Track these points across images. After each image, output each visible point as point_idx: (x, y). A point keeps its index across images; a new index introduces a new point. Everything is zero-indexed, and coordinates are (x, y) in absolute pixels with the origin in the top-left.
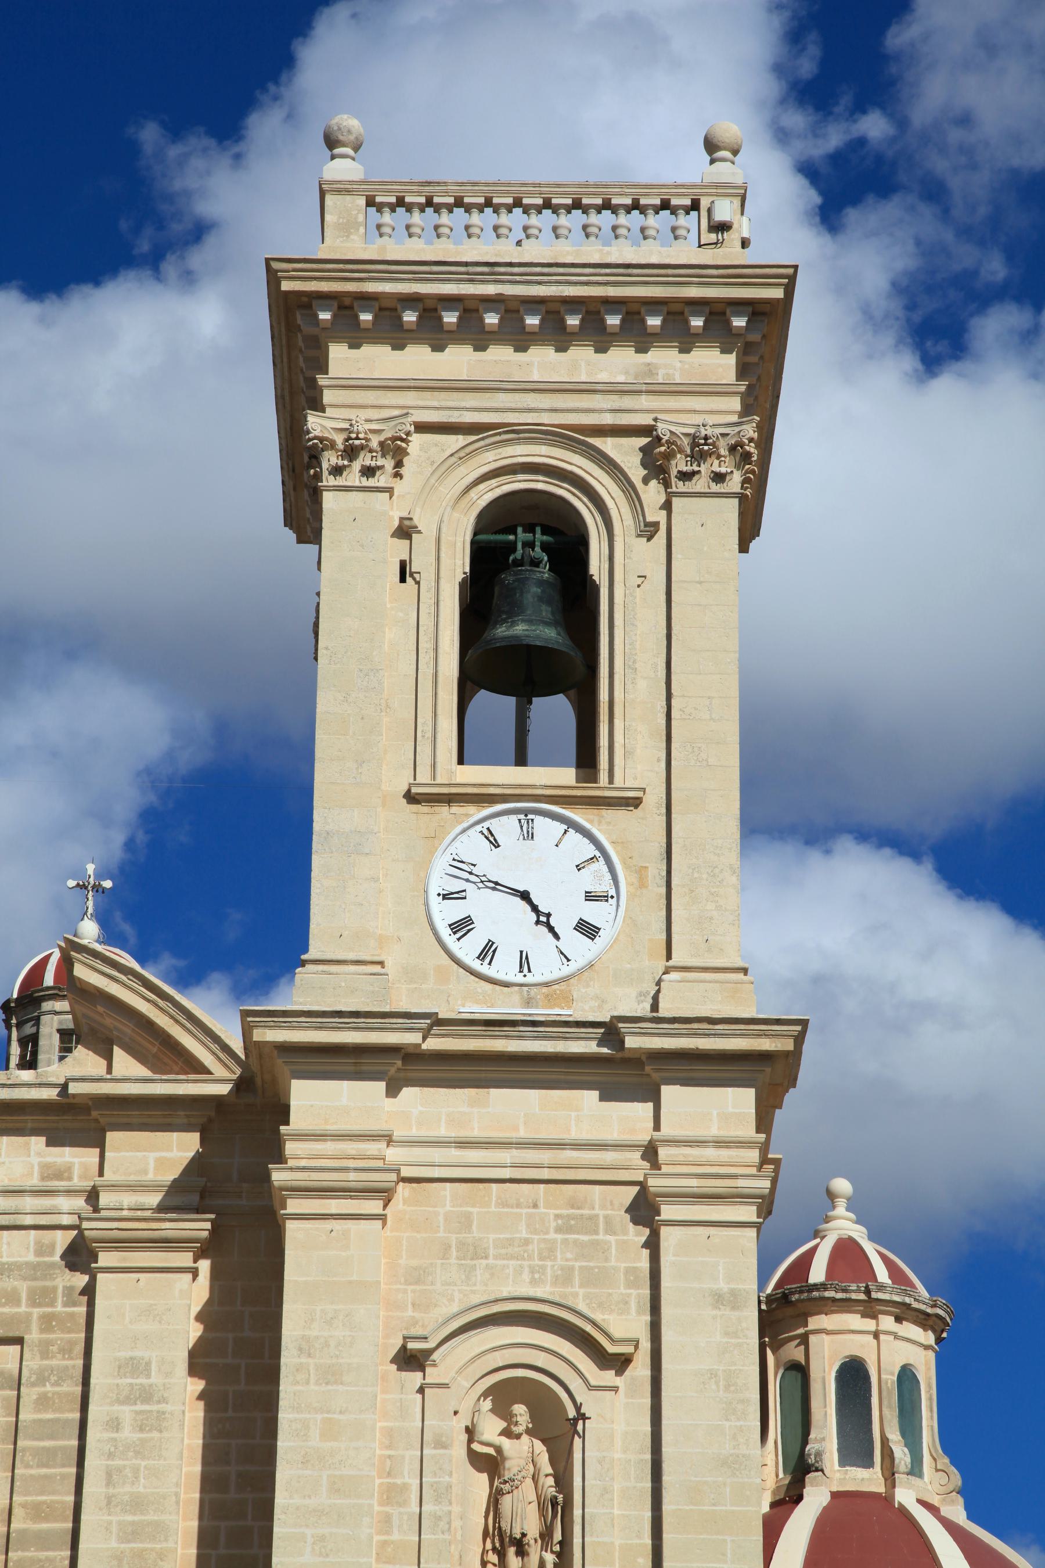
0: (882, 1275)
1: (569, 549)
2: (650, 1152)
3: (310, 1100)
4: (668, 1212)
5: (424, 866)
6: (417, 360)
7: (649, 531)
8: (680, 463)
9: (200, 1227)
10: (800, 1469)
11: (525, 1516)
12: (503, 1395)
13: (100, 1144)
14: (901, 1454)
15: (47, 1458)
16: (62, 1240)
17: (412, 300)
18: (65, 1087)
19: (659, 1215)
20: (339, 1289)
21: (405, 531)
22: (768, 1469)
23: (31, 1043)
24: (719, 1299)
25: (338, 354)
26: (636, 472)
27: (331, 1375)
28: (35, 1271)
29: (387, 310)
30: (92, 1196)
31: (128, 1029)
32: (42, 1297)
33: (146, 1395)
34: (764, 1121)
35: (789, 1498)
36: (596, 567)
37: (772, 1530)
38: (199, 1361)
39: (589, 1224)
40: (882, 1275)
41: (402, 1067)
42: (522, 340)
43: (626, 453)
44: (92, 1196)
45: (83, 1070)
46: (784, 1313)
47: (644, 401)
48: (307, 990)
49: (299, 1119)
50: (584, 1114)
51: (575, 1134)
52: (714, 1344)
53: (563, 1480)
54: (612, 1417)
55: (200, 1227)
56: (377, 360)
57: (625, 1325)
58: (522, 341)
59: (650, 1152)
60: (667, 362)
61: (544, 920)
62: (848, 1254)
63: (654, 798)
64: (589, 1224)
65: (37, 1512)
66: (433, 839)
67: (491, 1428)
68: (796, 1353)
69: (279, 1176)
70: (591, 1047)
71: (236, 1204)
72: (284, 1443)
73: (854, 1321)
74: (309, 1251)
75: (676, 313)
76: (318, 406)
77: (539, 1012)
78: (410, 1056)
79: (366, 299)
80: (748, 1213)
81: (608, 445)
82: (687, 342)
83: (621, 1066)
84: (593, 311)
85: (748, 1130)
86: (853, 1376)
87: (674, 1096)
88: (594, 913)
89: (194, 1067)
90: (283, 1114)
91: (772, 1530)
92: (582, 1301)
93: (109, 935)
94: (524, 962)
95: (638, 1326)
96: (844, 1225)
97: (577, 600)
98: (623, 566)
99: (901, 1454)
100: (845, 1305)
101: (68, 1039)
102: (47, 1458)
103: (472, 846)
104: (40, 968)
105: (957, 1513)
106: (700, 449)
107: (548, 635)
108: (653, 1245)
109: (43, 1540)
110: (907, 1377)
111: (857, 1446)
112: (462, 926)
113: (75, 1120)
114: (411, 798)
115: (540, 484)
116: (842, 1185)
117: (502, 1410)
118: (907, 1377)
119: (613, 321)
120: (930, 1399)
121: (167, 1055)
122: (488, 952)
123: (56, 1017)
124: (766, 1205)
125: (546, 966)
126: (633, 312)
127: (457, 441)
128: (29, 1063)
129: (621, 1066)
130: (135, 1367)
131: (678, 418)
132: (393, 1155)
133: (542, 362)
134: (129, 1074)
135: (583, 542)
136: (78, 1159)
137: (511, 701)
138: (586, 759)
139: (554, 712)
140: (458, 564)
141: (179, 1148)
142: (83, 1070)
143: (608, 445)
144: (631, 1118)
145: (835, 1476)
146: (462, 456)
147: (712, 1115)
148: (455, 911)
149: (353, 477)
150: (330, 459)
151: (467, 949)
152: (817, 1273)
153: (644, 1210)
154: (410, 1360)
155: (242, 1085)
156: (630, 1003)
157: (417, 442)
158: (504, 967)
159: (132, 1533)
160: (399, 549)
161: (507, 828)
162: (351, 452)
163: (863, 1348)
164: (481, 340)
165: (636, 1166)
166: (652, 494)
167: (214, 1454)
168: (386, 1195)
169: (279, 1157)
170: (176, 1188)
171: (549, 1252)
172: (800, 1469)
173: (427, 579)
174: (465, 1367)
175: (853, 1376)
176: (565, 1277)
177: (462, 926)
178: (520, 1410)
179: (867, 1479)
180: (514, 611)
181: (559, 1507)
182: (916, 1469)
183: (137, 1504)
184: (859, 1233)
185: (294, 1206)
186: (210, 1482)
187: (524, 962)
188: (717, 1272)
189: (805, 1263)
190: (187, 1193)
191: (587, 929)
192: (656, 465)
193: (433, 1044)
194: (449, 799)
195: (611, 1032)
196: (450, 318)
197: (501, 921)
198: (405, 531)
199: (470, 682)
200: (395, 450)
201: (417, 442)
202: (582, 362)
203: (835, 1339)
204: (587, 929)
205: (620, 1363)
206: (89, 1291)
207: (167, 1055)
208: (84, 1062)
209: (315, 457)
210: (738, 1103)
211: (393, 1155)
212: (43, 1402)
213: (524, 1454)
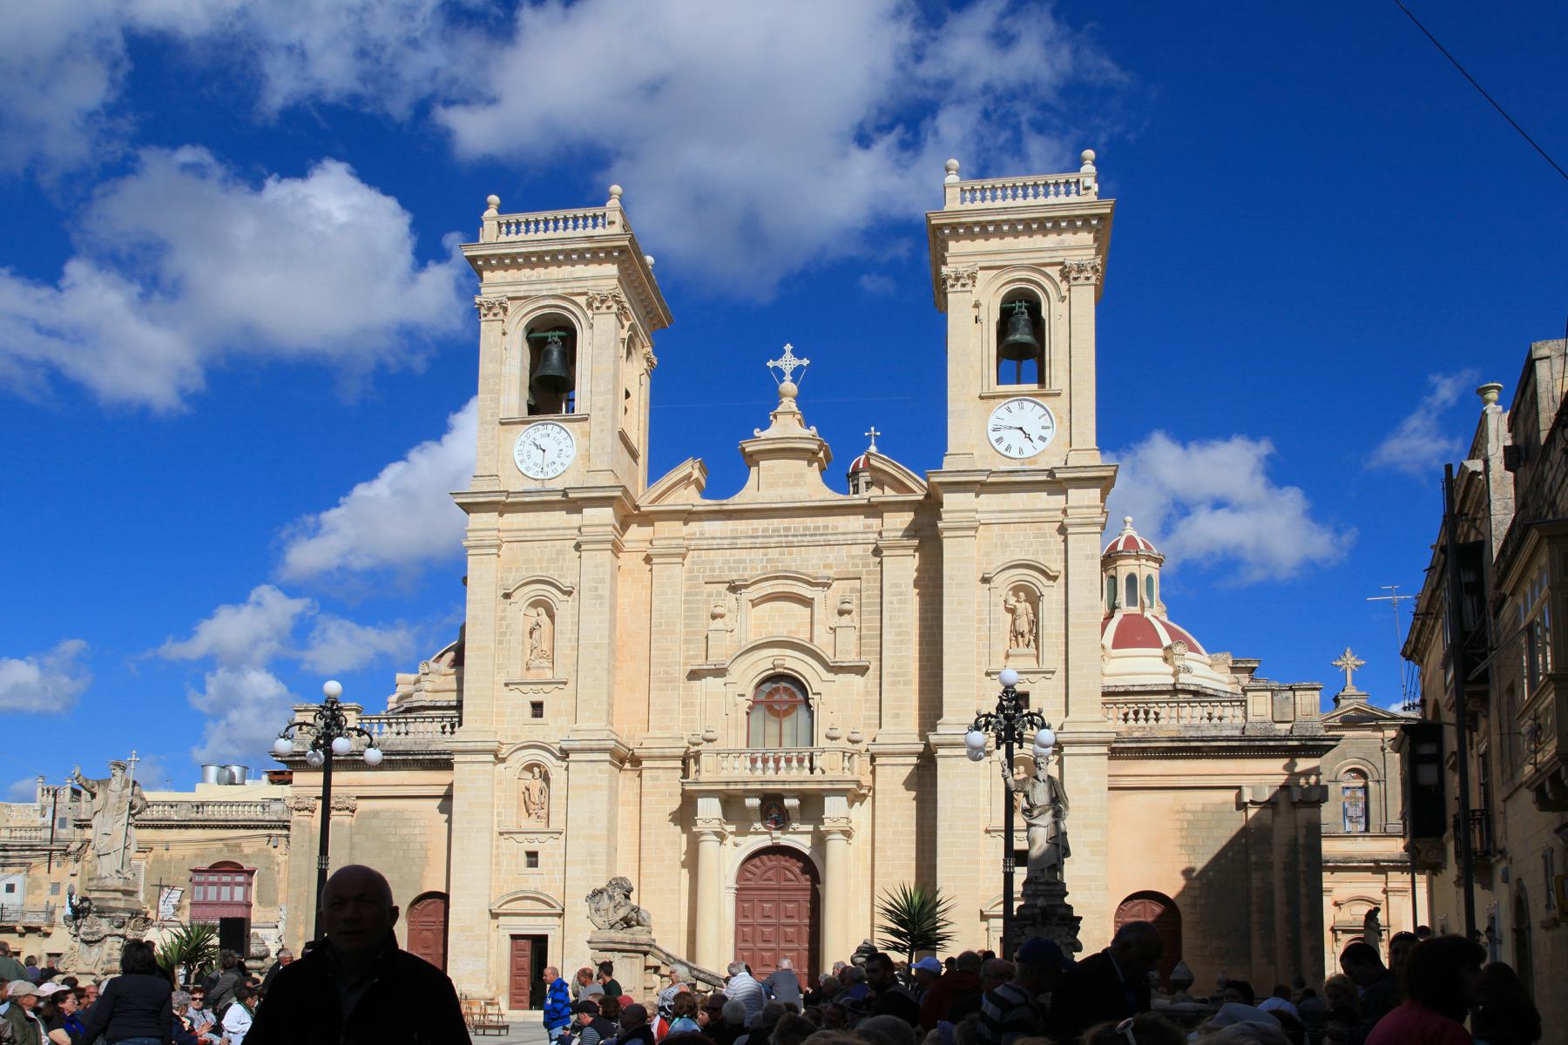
0: (1142, 546)
1: (1034, 307)
2: (1065, 511)
3: (950, 500)
4: (1070, 530)
6: (980, 245)
7: (1063, 299)
8: (1073, 274)
9: (916, 542)
10: (1113, 608)
11: (1023, 625)
12: (1016, 590)
14: (1147, 602)
15: (870, 613)
16: (871, 547)
19: (1079, 948)
20: (962, 559)
21: (977, 305)
22: (1103, 609)
23: (856, 486)
24: (1087, 557)
25: (952, 244)
26: (1058, 279)
27: (960, 586)
28: (863, 557)
29: (969, 227)
30: (880, 533)
31: (889, 480)
32: (866, 565)
33: (901, 594)
34: (1103, 499)
35: (1110, 617)
36: (1044, 313)
37: (1104, 627)
40: (1142, 546)
41: (980, 488)
42: (1016, 234)
43: (1054, 272)
44: (880, 533)
45: (875, 494)
46: (1109, 560)
47: (1061, 253)
48: (949, 464)
49: (946, 506)
50: (1041, 499)
51: (1039, 506)
52: (1086, 571)
53: (1036, 614)
54: (1052, 596)
55: (916, 542)
56: (965, 246)
57: (1056, 566)
58: (1016, 234)
59: (1065, 511)
60: (1068, 238)
61: (1028, 436)
62: (1131, 541)
63: (1065, 393)
65: (869, 629)
66: (990, 411)
67: (1012, 601)
68: (1112, 572)
69: (940, 525)
70: (1044, 478)
71: (927, 535)
72: (945, 607)
73: (1132, 561)
74: (952, 549)
75: (1071, 220)
76: (945, 263)
77: (1026, 467)
78: (983, 484)
79: (961, 224)
80: (1098, 529)
81: (1047, 270)
82: (1075, 230)
84: (1041, 222)
85: (1098, 503)
86: (1132, 579)
88: (1045, 433)
89: (911, 491)
90: (941, 505)
91: (1104, 627)
93: (880, 450)
94: (1021, 451)
95: (1061, 567)
96: (1130, 531)
98: (1053, 313)
99: (1147, 602)
100: (1129, 557)
101: (869, 485)
102: (870, 613)
103: (1003, 412)
105: (1165, 618)
106: (1081, 269)
107: (1028, 338)
108: (1065, 541)
109: (872, 637)
110: (1149, 578)
111: (1132, 600)
112: (999, 440)
113: (873, 510)
114: (981, 398)
115: (1024, 285)
116: (1129, 519)
117: (1016, 594)
118: (1149, 578)
119: (1049, 225)
121: (902, 487)
122: (1008, 448)
123: (864, 477)
124: (1103, 526)
125: (1028, 452)
126: (1056, 221)
127: (995, 272)
128: (856, 492)
129: (1055, 484)
130: (897, 585)
131: (1072, 259)
132: (978, 516)
133: (1024, 242)
134: (890, 494)
135: (1039, 305)
136: (875, 522)
137: (1014, 363)
138: (1041, 380)
139: (1030, 365)
140: (995, 315)
141: (907, 518)
142: (875, 494)
143: (1047, 270)
144: (1059, 501)
145: (1125, 609)
146: (996, 277)
148: (997, 435)
149: (958, 287)
150: (950, 282)
151: (1001, 448)
152: (1120, 548)
153: (1063, 530)
154: (985, 580)
155: (927, 496)
156: (1057, 462)
158: (1014, 453)
159: (899, 634)
161: (1014, 406)
162: (957, 279)
163: (1135, 570)
165: (1060, 517)
166: (1064, 286)
167: (923, 610)
168: (976, 529)
169: (940, 519)
170: (907, 530)
171: (1031, 545)
172: (1113, 608)
173: (985, 321)
174: (1003, 582)
175: (1132, 579)
177: (999, 440)
178: (1022, 594)
179: (1136, 610)
180: (1015, 330)
181: (1035, 623)
182: (1151, 606)
183: (900, 626)
184: (1134, 534)
185: (941, 752)
187: (1021, 451)
188: (1087, 549)
189: (1116, 544)
190: (911, 532)
191: (1043, 439)
192: (1065, 276)
193: (991, 480)
194: (994, 397)
195: (1051, 473)
196: (991, 229)
198: (977, 305)
199: (1000, 356)
200: (973, 277)
201: (980, 273)
202: (1038, 241)
203: (1124, 568)
204: (1043, 439)
205: (1055, 578)
206: (881, 563)
207: (902, 487)
209: (944, 282)
210: (1096, 492)
211: (978, 516)
212: (869, 629)
213: (1023, 607)
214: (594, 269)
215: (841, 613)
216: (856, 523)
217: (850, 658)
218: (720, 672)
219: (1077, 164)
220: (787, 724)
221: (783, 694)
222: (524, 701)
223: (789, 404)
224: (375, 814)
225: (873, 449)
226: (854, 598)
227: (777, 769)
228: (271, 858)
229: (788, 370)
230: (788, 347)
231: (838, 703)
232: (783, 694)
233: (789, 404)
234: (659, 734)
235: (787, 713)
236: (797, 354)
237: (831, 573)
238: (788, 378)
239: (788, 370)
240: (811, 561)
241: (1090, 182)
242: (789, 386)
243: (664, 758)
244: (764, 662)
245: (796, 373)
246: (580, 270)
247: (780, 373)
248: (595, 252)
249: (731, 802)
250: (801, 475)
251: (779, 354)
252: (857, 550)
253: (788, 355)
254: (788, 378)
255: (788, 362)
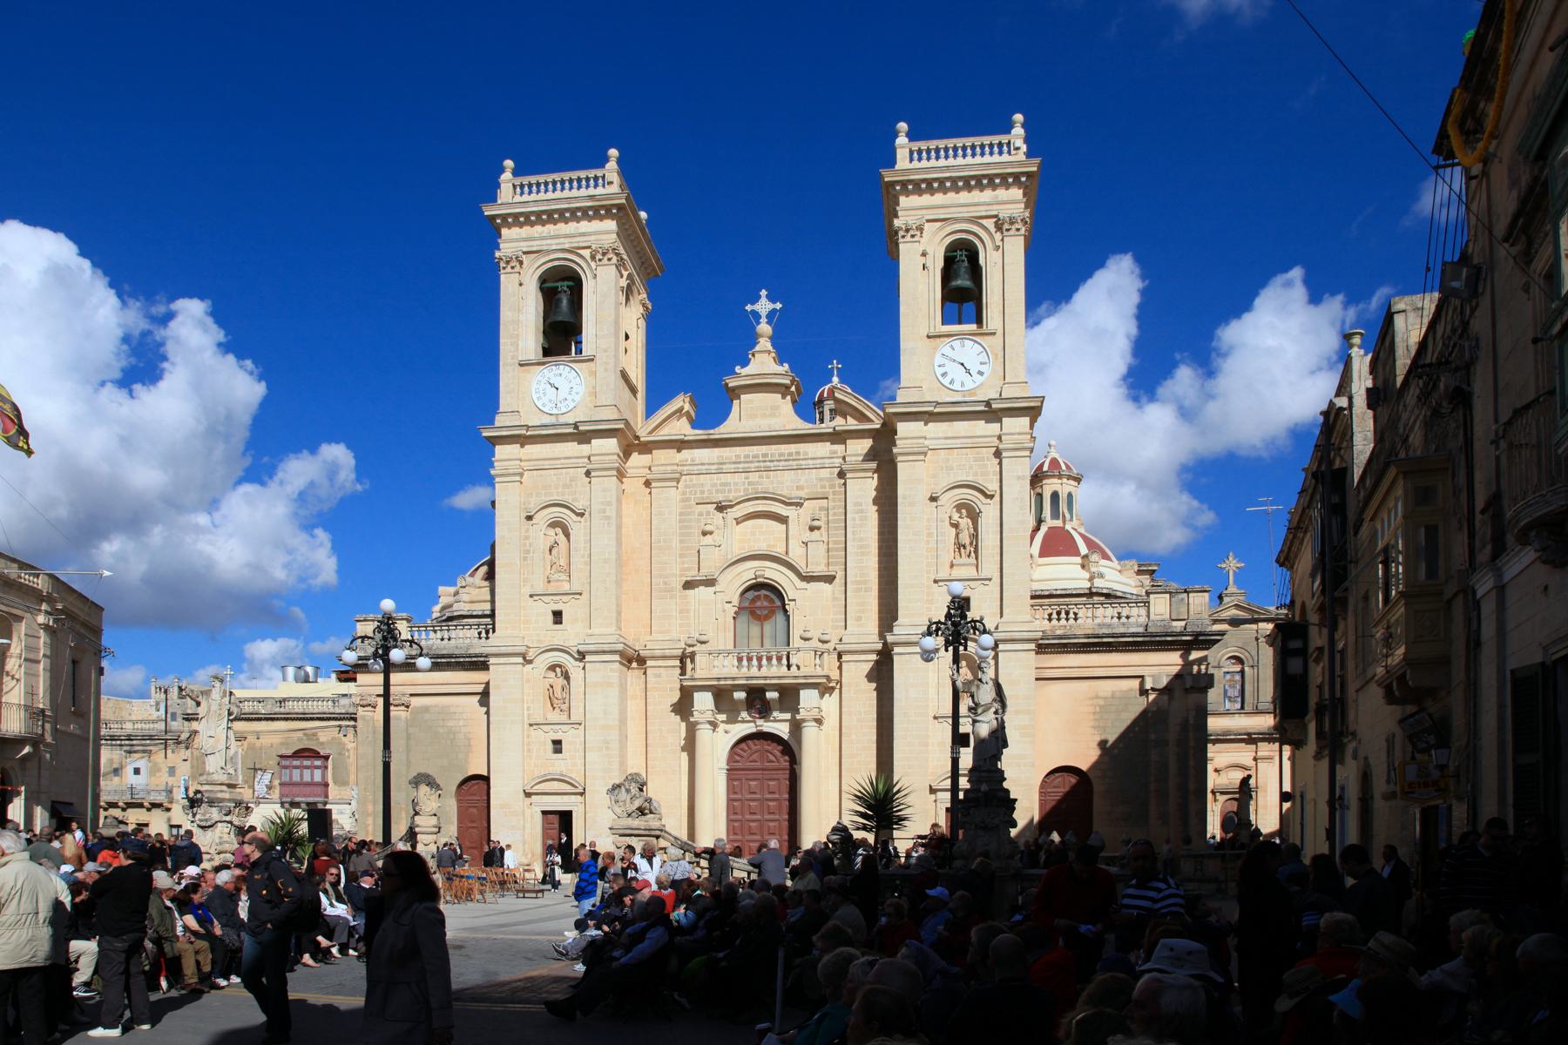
1: (973, 255)
2: (1000, 438)
3: (903, 428)
5: (933, 359)
6: (926, 199)
8: (1006, 226)
9: (874, 465)
10: (1040, 521)
11: (965, 538)
12: (959, 507)
13: (1000, 421)
14: (1068, 516)
15: (837, 529)
17: (924, 180)
18: (576, 427)
20: (912, 479)
21: (924, 254)
22: (1032, 523)
25: (902, 199)
26: (993, 229)
28: (831, 479)
32: (832, 486)
34: (1032, 427)
35: (1037, 529)
36: (982, 261)
38: (875, 501)
39: (982, 459)
43: (990, 224)
45: (839, 423)
50: (981, 427)
54: (989, 512)
55: (874, 465)
57: (992, 487)
59: (1000, 438)
60: (1002, 193)
61: (968, 371)
63: (1000, 332)
64: (982, 459)
65: (836, 542)
66: (936, 349)
67: (956, 516)
69: (895, 450)
70: (982, 408)
71: (883, 458)
75: (1004, 177)
76: (896, 216)
78: (931, 414)
79: (910, 181)
83: (991, 413)
85: (1027, 429)
86: (1055, 496)
87: (1007, 421)
88: (983, 368)
89: (870, 420)
92: (981, 481)
93: (841, 382)
95: (996, 487)
97: (976, 272)
98: (989, 260)
99: (1068, 516)
103: (947, 350)
104: (1041, 466)
106: (1012, 221)
108: (1000, 464)
111: (1055, 514)
113: (838, 437)
114: (936, 581)
115: (964, 236)
117: (959, 511)
120: (1501, 706)
121: (862, 417)
125: (969, 385)
127: (938, 224)
129: (991, 413)
131: (1005, 212)
132: (927, 442)
133: (964, 197)
135: (977, 253)
136: (839, 448)
139: (969, 307)
140: (940, 263)
141: (867, 443)
142: (839, 423)
143: (984, 222)
144: (994, 428)
145: (1050, 522)
146: (940, 229)
147: (1016, 426)
149: (908, 238)
150: (901, 233)
151: (946, 382)
152: (1045, 468)
154: (933, 499)
155: (884, 425)
157: (927, 226)
158: (957, 386)
159: (861, 547)
160: (923, 260)
161: (957, 344)
162: (907, 230)
163: (1057, 488)
164: (945, 191)
165: (996, 442)
166: (998, 236)
168: (925, 454)
170: (867, 455)
172: (1040, 521)
174: (948, 500)
175: (1055, 496)
176: (976, 474)
177: (944, 375)
179: (1058, 523)
180: (957, 276)
181: (975, 536)
183: (861, 539)
184: (1057, 456)
186: (880, 533)
188: (1018, 470)
190: (870, 456)
191: (981, 373)
192: (999, 227)
195: (988, 403)
197: (956, 373)
200: (920, 229)
201: (927, 226)
204: (981, 373)
205: (991, 497)
207: (862, 417)
208: (839, 421)
210: (1026, 421)
213: (965, 523)
214: (596, 225)
215: (812, 529)
216: (824, 449)
217: (819, 568)
218: (710, 582)
219: (1007, 128)
220: (768, 627)
221: (763, 601)
222: (545, 610)
223: (764, 344)
224: (426, 709)
225: (835, 379)
226: (823, 514)
227: (760, 666)
228: (342, 745)
229: (764, 313)
230: (764, 293)
231: (811, 608)
232: (763, 601)
233: (764, 344)
234: (660, 637)
235: (767, 617)
236: (771, 298)
237: (803, 494)
238: (764, 320)
239: (764, 313)
240: (785, 483)
241: (1019, 143)
242: (764, 328)
243: (664, 657)
244: (746, 573)
245: (771, 315)
246: (584, 226)
247: (757, 315)
248: (596, 209)
249: (721, 695)
250: (775, 408)
251: (756, 299)
252: (824, 473)
253: (764, 300)
254: (764, 320)
255: (764, 306)
